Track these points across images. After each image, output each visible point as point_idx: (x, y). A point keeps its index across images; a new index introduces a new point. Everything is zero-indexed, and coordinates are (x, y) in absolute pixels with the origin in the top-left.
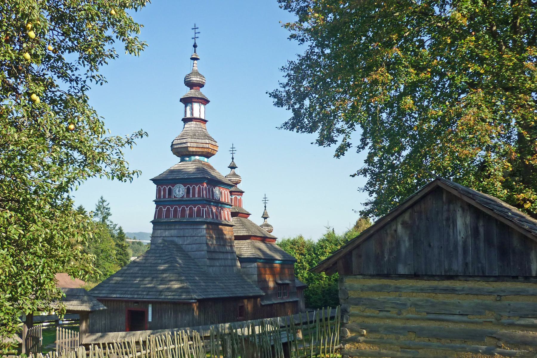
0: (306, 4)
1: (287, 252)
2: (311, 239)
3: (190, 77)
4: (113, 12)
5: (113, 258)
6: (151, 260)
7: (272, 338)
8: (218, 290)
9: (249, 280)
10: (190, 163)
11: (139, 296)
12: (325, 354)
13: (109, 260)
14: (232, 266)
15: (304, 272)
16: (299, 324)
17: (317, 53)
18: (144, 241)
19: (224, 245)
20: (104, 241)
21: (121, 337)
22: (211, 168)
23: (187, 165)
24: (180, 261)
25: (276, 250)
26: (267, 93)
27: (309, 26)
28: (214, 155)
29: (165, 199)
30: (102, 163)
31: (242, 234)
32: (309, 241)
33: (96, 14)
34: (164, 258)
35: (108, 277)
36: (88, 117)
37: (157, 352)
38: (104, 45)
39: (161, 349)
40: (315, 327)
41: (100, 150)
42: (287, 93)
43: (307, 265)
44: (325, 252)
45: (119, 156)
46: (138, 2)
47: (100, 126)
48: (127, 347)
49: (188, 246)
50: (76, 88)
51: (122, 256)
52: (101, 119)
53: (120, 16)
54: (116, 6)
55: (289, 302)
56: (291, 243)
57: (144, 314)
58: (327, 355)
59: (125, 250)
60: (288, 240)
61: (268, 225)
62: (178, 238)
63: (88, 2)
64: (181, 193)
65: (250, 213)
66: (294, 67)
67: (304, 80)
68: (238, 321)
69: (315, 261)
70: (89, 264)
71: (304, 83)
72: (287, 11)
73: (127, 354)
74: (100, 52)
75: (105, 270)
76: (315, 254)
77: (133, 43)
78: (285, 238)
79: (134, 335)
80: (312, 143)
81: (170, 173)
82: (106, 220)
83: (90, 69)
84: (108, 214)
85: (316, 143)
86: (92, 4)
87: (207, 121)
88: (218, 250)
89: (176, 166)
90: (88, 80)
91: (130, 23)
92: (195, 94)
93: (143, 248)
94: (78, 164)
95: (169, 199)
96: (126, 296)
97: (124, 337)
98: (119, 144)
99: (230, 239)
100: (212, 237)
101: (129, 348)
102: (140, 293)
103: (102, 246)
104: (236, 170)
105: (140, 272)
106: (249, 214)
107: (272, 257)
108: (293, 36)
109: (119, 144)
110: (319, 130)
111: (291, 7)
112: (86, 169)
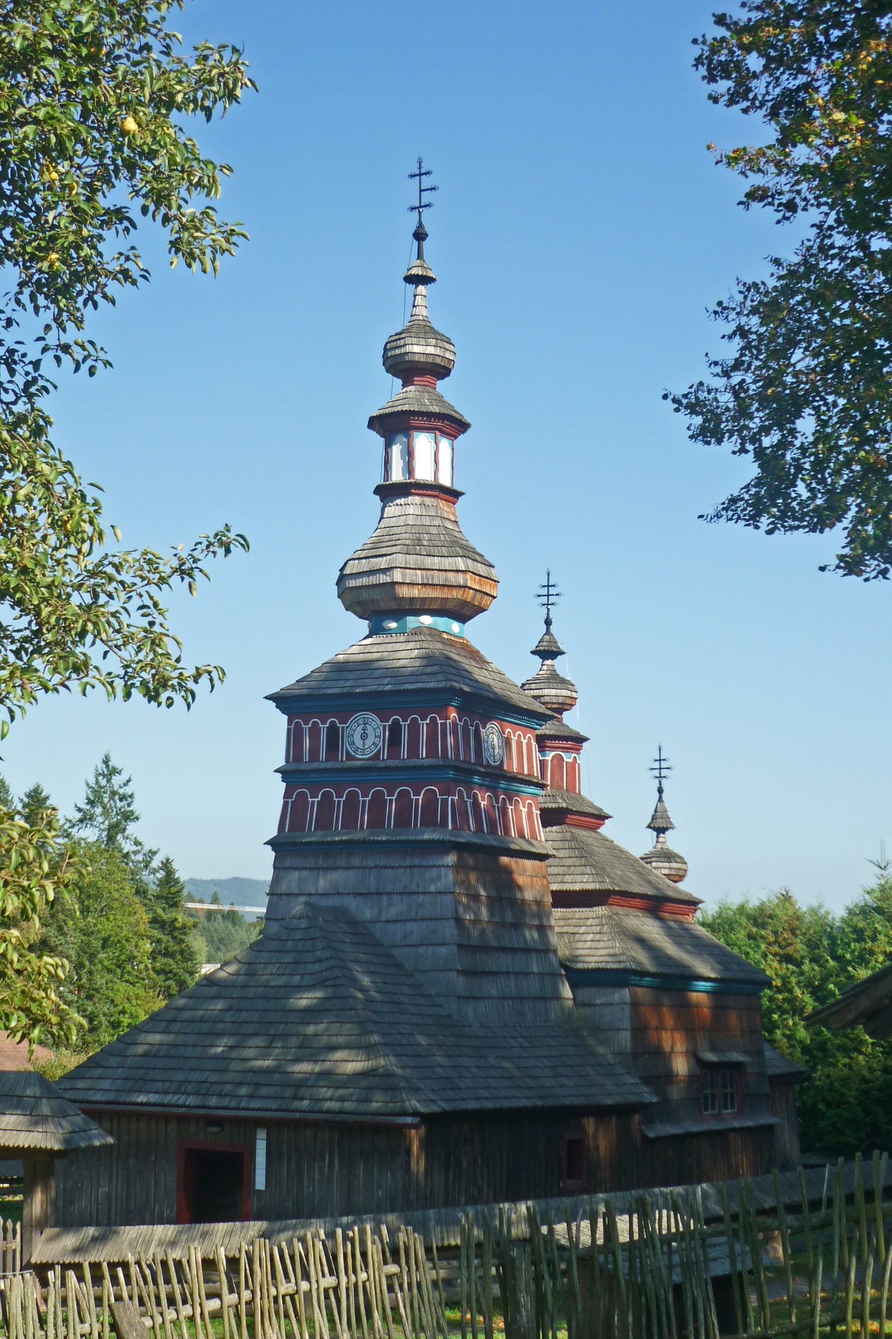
0: (802, 79)
1: (736, 951)
2: (820, 906)
3: (402, 342)
4: (131, 125)
5: (142, 966)
6: (269, 975)
7: (676, 1259)
8: (493, 1083)
9: (601, 1050)
10: (402, 638)
11: (226, 1101)
12: (863, 1324)
13: (129, 973)
14: (544, 999)
15: (795, 1024)
16: (772, 1212)
17: (842, 248)
18: (248, 909)
19: (518, 926)
20: (111, 908)
21: (160, 1243)
22: (475, 655)
23: (390, 647)
24: (366, 981)
25: (699, 946)
26: (665, 397)
27: (813, 154)
28: (483, 610)
29: (315, 765)
30: (93, 643)
31: (577, 887)
32: (813, 911)
33: (75, 132)
34: (310, 968)
35: (123, 1031)
36: (47, 486)
37: (276, 1299)
38: (100, 238)
39: (290, 1288)
40: (827, 1223)
41: (88, 599)
42: (736, 394)
43: (808, 999)
44: (872, 953)
45: (150, 619)
46: (215, 89)
47: (86, 517)
48: (174, 1280)
49: (391, 927)
50: (6, 386)
51: (171, 961)
52: (91, 493)
53: (154, 138)
54: (140, 103)
55: (741, 1130)
56: (750, 917)
57: (243, 1162)
58: (873, 1326)
59: (182, 941)
60: (742, 909)
61: (668, 856)
62: (360, 899)
63: (48, 95)
64: (369, 742)
65: (607, 810)
66: (760, 302)
67: (795, 344)
68: (562, 1193)
69: (836, 985)
70: (45, 990)
71: (798, 354)
72: (736, 108)
73: (172, 1302)
74: (86, 261)
75: (112, 1009)
76: (835, 957)
77: (198, 229)
78: (729, 900)
79: (204, 1235)
80: (822, 569)
81: (335, 675)
82: (119, 837)
83: (55, 320)
84: (128, 816)
85: (838, 567)
86: (64, 99)
87: (461, 494)
88: (493, 943)
89: (355, 649)
90: (48, 360)
91: (187, 159)
92: (418, 400)
93: (242, 934)
94: (14, 647)
95: (330, 765)
96: (181, 1099)
97: (173, 1244)
98: (151, 576)
99: (539, 903)
100: (476, 897)
101: (179, 1282)
102: (228, 1088)
103: (106, 927)
104: (560, 665)
105: (228, 1016)
106: (602, 817)
107: (685, 967)
108: (757, 195)
109: (151, 576)
110: (846, 522)
111: (751, 96)
112: (38, 663)
